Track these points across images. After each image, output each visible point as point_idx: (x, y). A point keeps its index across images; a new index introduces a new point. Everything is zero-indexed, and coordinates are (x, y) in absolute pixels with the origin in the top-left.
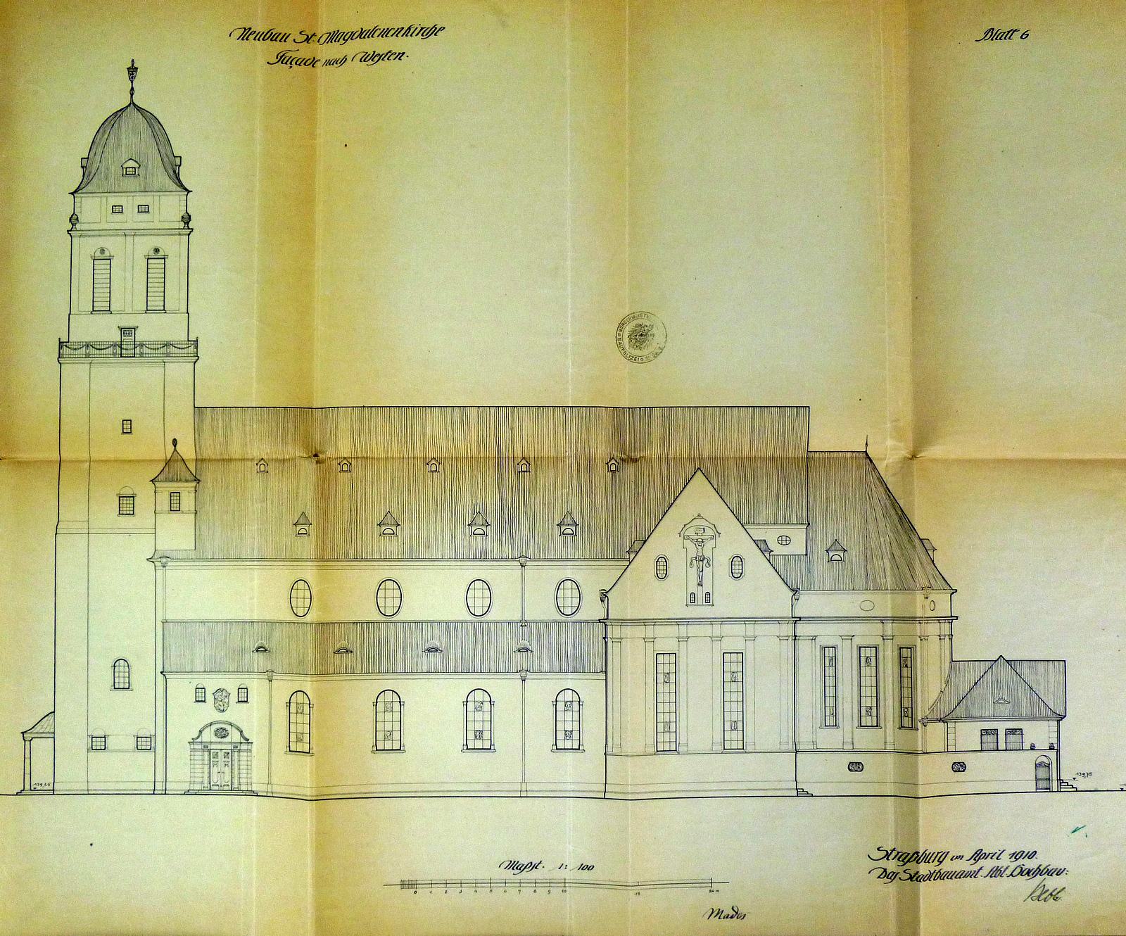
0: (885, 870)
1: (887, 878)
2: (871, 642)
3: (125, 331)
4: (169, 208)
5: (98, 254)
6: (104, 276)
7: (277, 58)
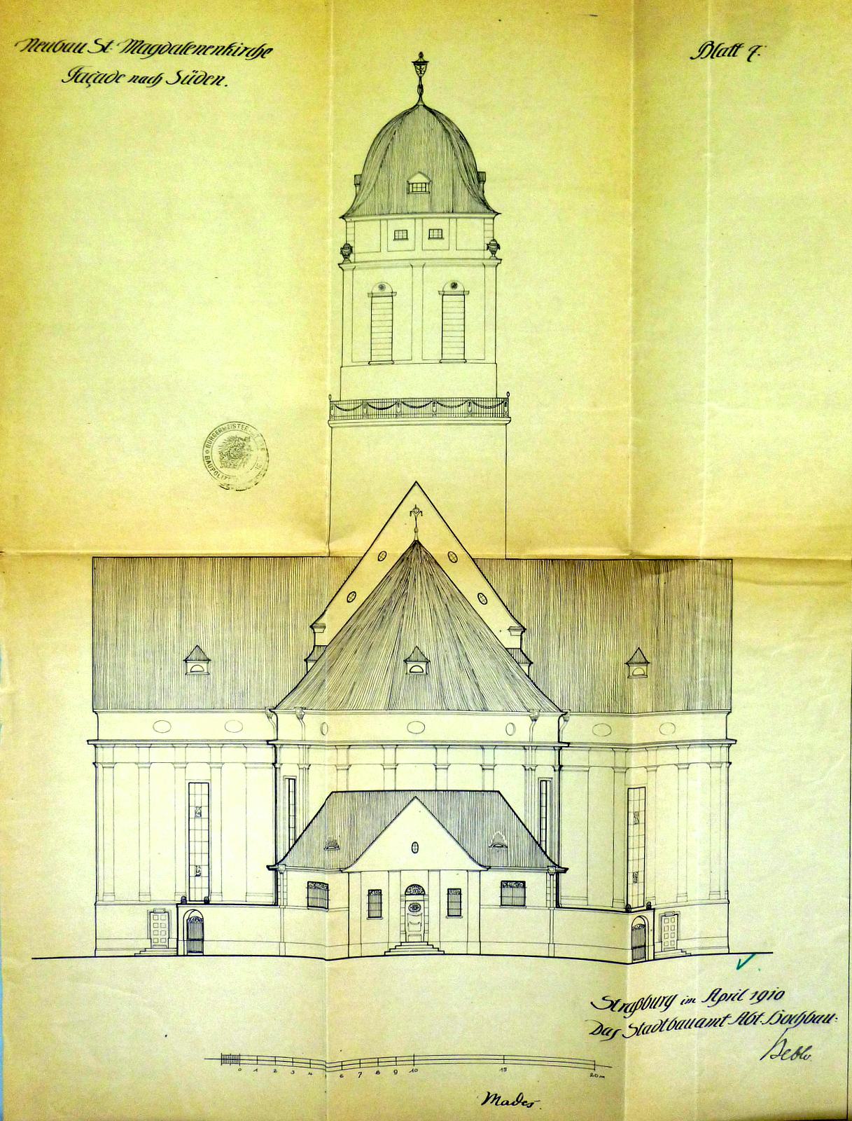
4: (472, 232)
5: (376, 290)
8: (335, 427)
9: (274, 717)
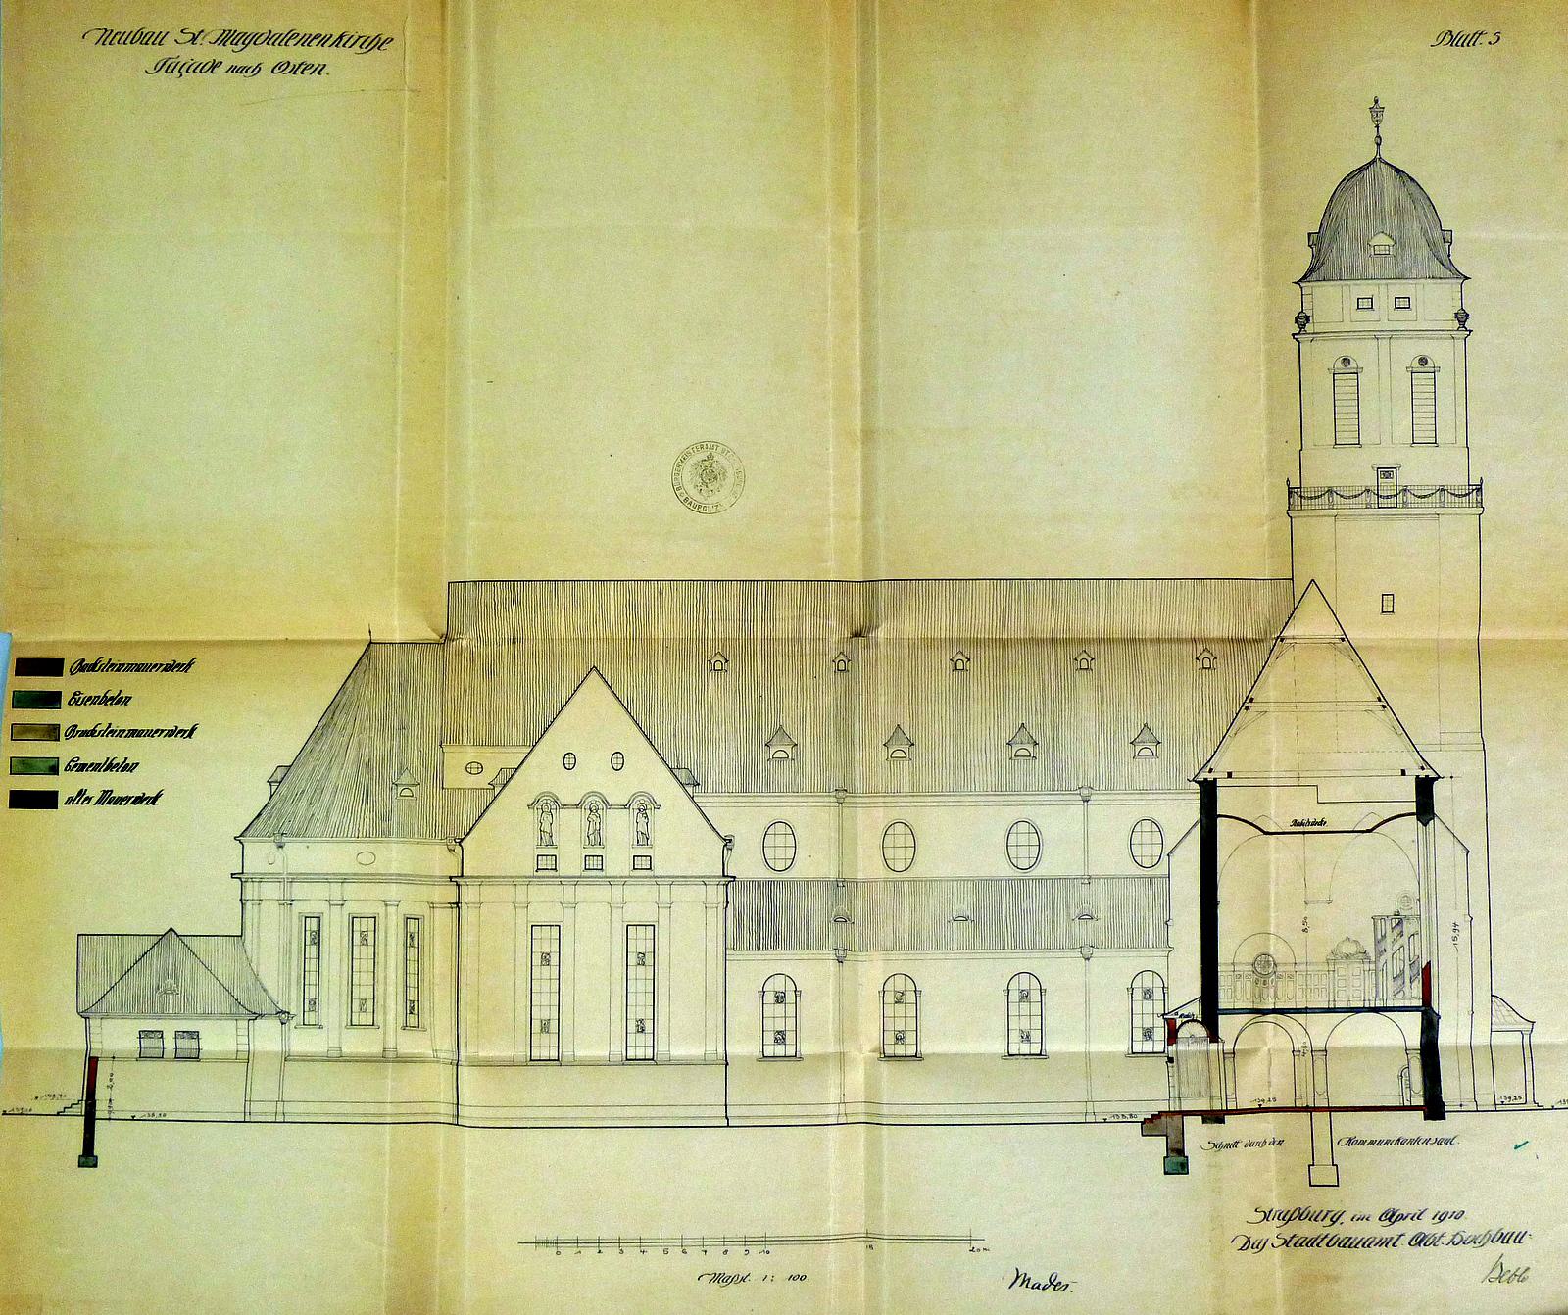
0: (1249, 1239)
2: (369, 911)
3: (1386, 473)
4: (1435, 300)
9: (458, 849)
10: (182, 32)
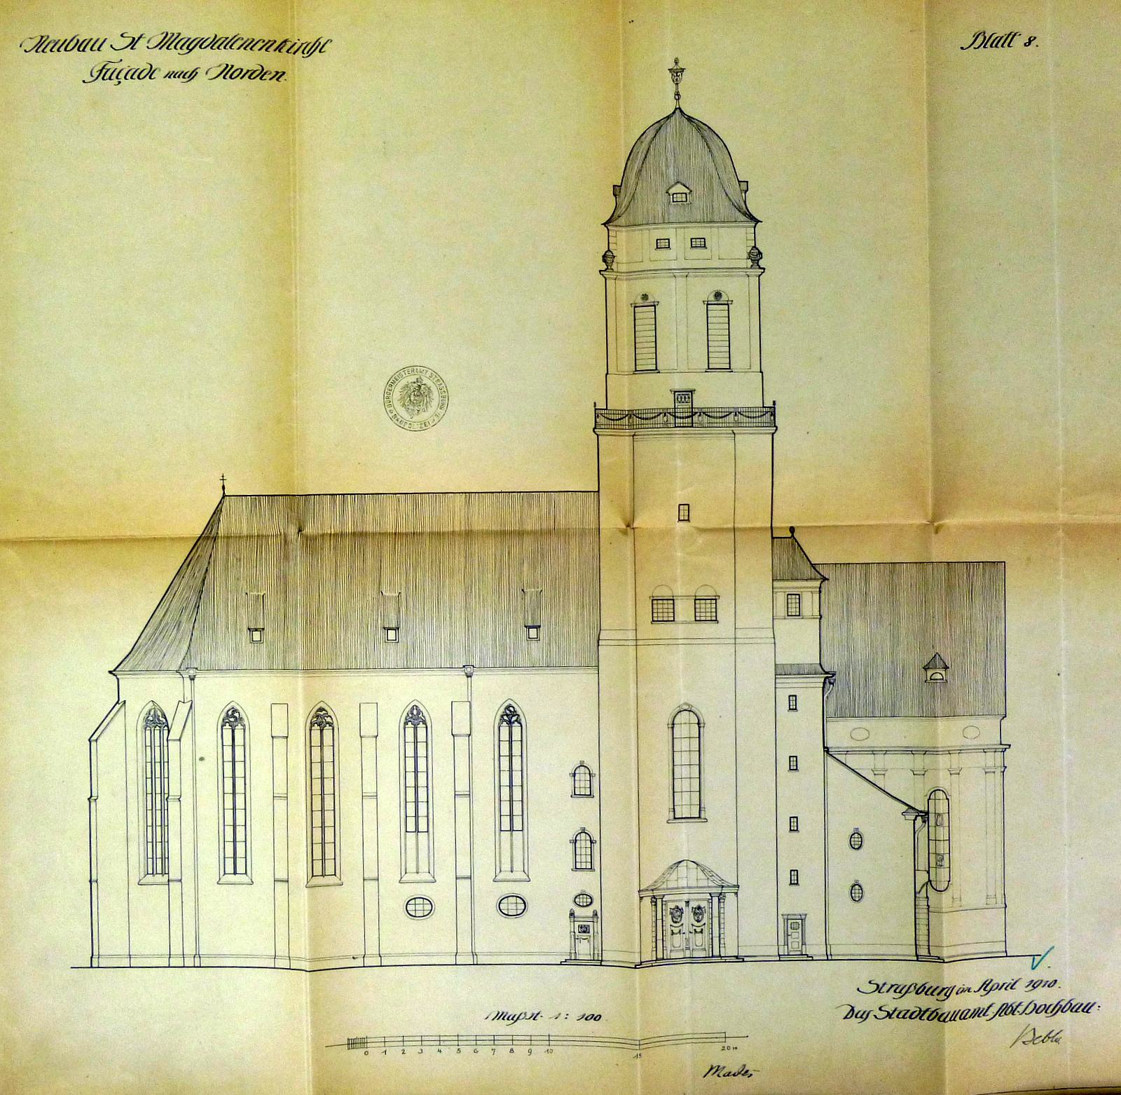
1: (856, 1017)
5: (639, 301)
6: (648, 327)
7: (197, 73)
8: (602, 435)
10: (122, 35)
